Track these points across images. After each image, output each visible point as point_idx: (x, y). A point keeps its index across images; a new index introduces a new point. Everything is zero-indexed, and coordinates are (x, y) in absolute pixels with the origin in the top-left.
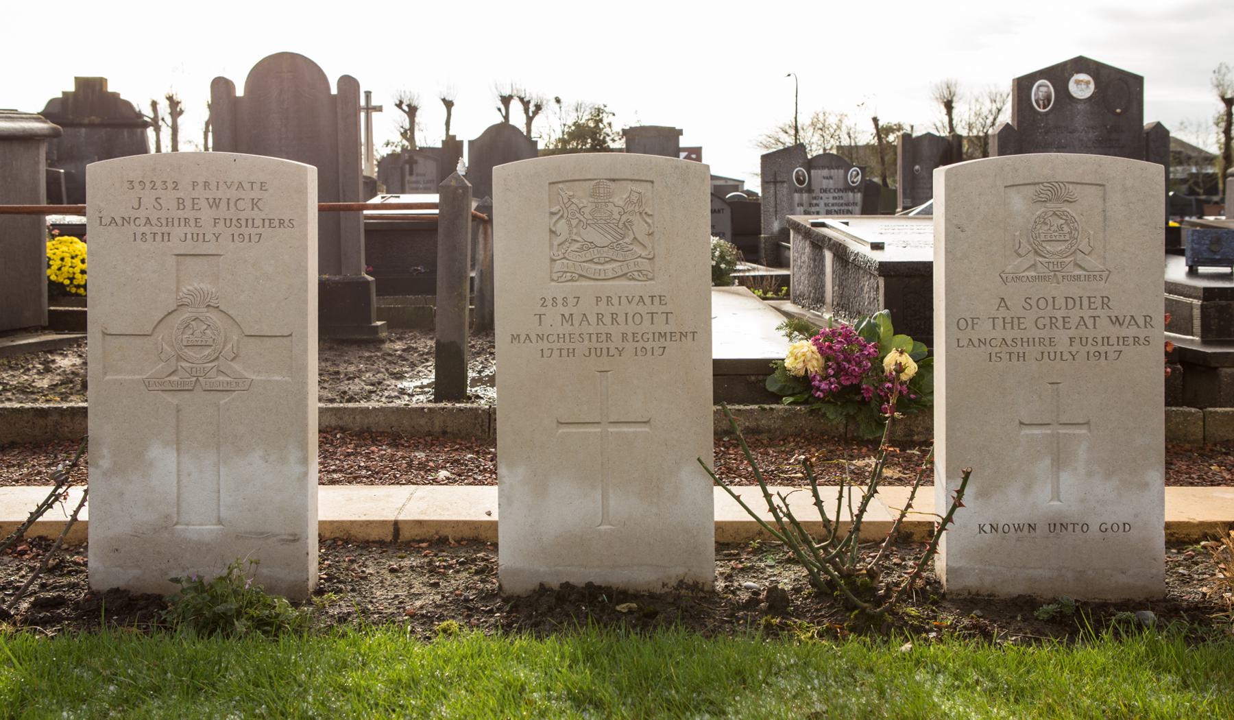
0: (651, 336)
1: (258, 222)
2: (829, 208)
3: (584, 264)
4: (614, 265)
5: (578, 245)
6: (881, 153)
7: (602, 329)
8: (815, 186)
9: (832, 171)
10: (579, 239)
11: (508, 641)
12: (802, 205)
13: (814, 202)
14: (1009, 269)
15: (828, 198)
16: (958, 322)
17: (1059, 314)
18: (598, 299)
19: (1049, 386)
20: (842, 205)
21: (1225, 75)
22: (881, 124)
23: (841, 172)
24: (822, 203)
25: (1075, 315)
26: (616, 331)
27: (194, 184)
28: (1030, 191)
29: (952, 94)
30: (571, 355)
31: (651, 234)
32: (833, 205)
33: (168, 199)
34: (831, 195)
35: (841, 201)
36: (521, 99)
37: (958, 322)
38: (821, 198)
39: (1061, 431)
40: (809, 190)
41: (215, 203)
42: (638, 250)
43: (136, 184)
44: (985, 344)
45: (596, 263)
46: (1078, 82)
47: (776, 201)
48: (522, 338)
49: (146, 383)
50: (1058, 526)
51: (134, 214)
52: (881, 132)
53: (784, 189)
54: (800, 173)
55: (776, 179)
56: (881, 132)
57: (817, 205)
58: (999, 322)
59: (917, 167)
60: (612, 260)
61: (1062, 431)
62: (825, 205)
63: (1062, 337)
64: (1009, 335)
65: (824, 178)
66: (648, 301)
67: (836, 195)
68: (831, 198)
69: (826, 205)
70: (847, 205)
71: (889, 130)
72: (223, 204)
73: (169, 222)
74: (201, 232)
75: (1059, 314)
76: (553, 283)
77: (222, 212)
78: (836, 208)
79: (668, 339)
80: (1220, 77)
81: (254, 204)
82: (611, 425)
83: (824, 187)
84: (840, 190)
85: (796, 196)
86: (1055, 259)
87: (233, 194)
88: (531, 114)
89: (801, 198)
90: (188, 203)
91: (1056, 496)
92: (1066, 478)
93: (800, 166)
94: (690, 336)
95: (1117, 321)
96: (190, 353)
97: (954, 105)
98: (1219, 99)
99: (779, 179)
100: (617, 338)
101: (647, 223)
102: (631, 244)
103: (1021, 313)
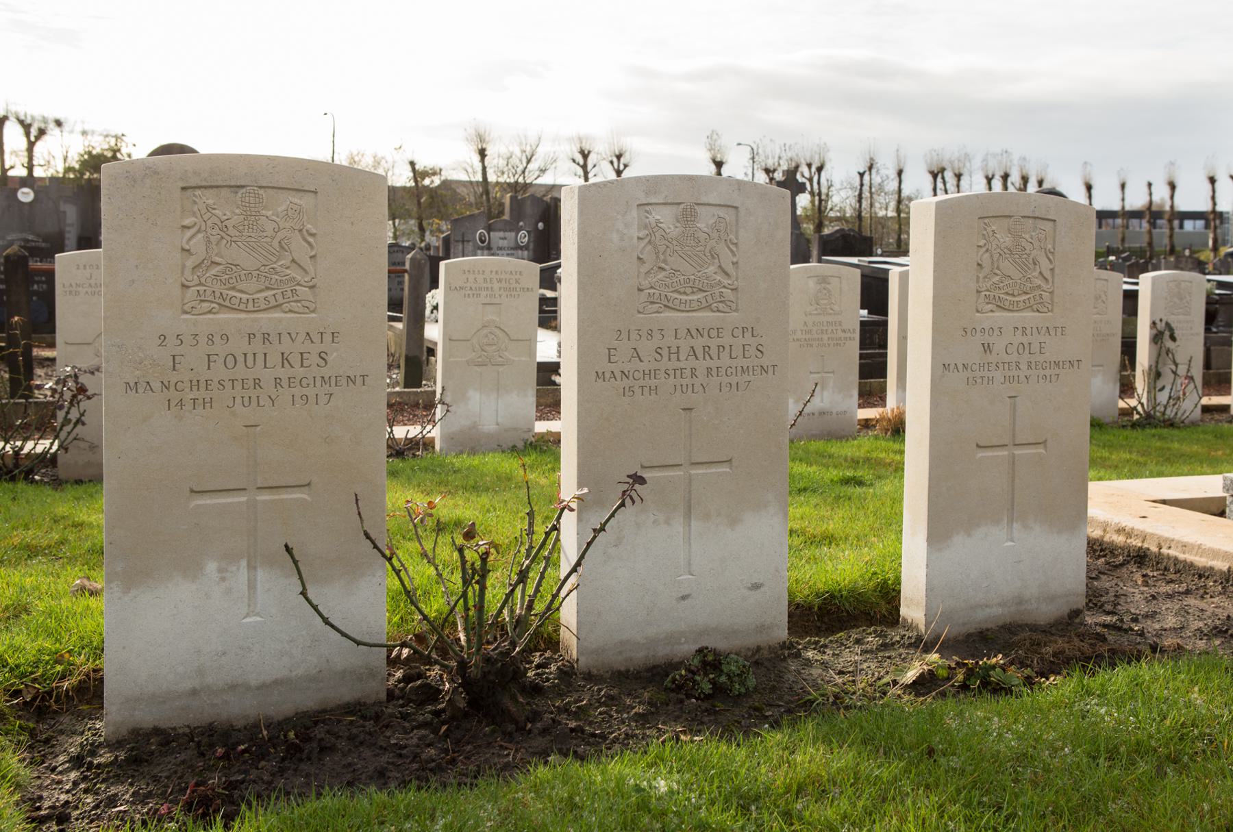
0: (1048, 365)
1: (518, 289)
3: (227, 292)
4: (700, 295)
6: (417, 196)
8: (494, 245)
9: (506, 233)
14: (808, 310)
16: (235, 363)
17: (824, 328)
18: (251, 336)
19: (244, 428)
21: (716, 140)
22: (417, 167)
23: (513, 234)
25: (830, 328)
26: (267, 376)
27: (491, 272)
28: (815, 279)
29: (481, 138)
30: (991, 382)
31: (1052, 270)
33: (480, 278)
36: (21, 122)
37: (235, 363)
39: (693, 472)
41: (500, 281)
44: (966, 369)
48: (952, 367)
49: (468, 362)
50: (822, 413)
51: (465, 285)
52: (418, 175)
55: (463, 238)
56: (418, 175)
58: (804, 332)
60: (700, 290)
61: (825, 375)
63: (825, 337)
64: (807, 337)
66: (317, 338)
67: (509, 252)
71: (425, 174)
72: (504, 282)
73: (480, 289)
75: (824, 328)
76: (978, 314)
77: (503, 285)
79: (751, 373)
80: (712, 143)
81: (517, 282)
83: (500, 246)
84: (512, 249)
87: (508, 276)
88: (33, 139)
90: (489, 280)
91: (822, 401)
92: (825, 393)
95: (844, 331)
96: (487, 348)
97: (486, 153)
98: (711, 161)
99: (466, 239)
100: (702, 373)
101: (309, 243)
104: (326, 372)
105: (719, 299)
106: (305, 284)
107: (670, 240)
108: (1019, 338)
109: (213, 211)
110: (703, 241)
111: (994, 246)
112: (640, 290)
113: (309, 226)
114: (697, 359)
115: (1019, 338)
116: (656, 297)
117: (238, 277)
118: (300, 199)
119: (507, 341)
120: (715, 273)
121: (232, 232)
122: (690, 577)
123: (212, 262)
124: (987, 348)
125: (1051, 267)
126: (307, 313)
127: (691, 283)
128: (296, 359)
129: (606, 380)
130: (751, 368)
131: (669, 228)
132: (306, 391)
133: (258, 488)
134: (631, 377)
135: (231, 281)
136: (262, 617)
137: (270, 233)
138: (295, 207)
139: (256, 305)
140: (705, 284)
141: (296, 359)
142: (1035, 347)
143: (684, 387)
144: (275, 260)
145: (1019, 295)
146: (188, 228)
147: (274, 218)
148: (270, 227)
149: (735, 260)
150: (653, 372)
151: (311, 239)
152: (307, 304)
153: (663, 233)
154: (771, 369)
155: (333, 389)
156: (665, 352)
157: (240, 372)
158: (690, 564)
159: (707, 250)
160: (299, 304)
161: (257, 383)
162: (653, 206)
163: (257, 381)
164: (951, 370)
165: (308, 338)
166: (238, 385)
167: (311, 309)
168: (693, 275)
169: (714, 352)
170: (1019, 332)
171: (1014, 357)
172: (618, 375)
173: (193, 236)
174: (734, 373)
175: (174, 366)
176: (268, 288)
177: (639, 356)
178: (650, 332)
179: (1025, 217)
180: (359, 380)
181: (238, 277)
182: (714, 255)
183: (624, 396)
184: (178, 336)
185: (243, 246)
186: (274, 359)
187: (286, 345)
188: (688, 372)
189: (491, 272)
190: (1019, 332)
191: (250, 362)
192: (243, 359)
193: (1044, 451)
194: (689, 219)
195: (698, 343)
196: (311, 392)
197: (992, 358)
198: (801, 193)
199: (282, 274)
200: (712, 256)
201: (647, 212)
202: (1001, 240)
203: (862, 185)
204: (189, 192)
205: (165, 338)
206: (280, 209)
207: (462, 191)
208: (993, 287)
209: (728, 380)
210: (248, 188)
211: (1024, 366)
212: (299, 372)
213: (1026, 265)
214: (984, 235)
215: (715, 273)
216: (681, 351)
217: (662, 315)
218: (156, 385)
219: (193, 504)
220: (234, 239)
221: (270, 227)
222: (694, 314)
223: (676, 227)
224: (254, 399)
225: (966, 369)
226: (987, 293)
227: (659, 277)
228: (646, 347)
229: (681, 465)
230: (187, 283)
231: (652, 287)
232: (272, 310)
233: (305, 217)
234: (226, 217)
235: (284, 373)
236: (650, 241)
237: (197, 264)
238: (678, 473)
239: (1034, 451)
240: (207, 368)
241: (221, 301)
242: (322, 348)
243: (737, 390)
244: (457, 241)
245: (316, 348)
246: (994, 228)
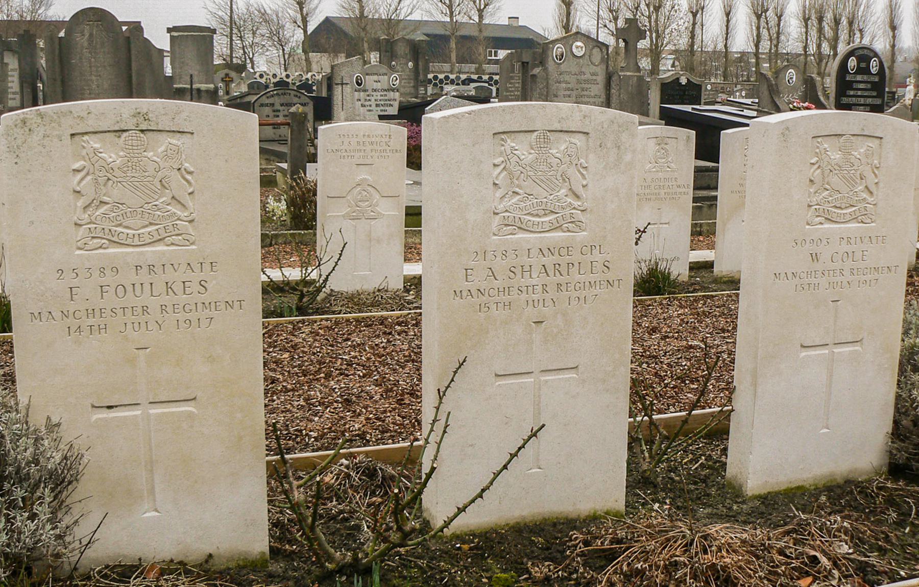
2: (378, 103)
3: (525, 217)
4: (552, 217)
12: (360, 100)
20: (386, 100)
24: (373, 99)
25: (667, 184)
26: (154, 303)
27: (364, 135)
32: (380, 100)
34: (379, 94)
35: (386, 98)
39: (152, 411)
41: (372, 143)
43: (341, 136)
46: (577, 47)
60: (851, 205)
62: (376, 100)
63: (662, 192)
64: (647, 191)
66: (197, 267)
67: (382, 93)
68: (379, 96)
69: (376, 100)
70: (389, 100)
74: (366, 154)
75: (662, 184)
76: (807, 227)
78: (382, 103)
79: (506, 294)
84: (385, 90)
86: (661, 164)
95: (679, 186)
101: (187, 181)
103: (650, 184)
104: (206, 298)
106: (185, 219)
107: (524, 166)
108: (845, 247)
109: (100, 155)
110: (554, 165)
111: (826, 163)
112: (496, 214)
113: (187, 165)
114: (548, 275)
115: (845, 247)
117: (124, 215)
118: (179, 140)
119: (378, 197)
120: (566, 196)
121: (117, 173)
122: (539, 470)
123: (101, 202)
124: (815, 257)
125: (876, 181)
126: (187, 246)
127: (544, 205)
128: (178, 287)
129: (464, 298)
130: (598, 283)
131: (524, 155)
133: (150, 403)
134: (487, 294)
135: (118, 218)
136: (159, 512)
137: (151, 171)
138: (174, 148)
139: (141, 239)
140: (557, 206)
141: (178, 287)
142: (858, 255)
143: (536, 301)
144: (157, 197)
146: (78, 171)
147: (155, 158)
148: (151, 168)
149: (584, 183)
150: (507, 289)
151: (189, 177)
152: (187, 237)
153: (518, 160)
154: (616, 283)
155: (214, 313)
156: (518, 271)
157: (130, 300)
158: (538, 460)
159: (559, 174)
160: (180, 238)
161: (145, 309)
162: (508, 135)
163: (145, 308)
164: (781, 278)
165: (189, 268)
166: (129, 312)
167: (191, 242)
168: (546, 198)
169: (564, 269)
170: (844, 242)
171: (838, 265)
172: (474, 292)
173: (82, 179)
174: (582, 288)
175: (72, 297)
176: (151, 224)
177: (494, 275)
178: (504, 252)
179: (854, 135)
181: (124, 215)
182: (565, 178)
183: (480, 312)
184: (74, 270)
185: (128, 186)
186: (160, 287)
187: (170, 275)
188: (539, 289)
189: (364, 135)
190: (844, 242)
191: (138, 292)
192: (132, 289)
193: (860, 349)
194: (542, 146)
195: (549, 260)
196: (193, 316)
197: (819, 266)
198: (641, 39)
199: (165, 210)
200: (564, 180)
201: (502, 140)
202: (832, 157)
203: (694, 24)
204: (77, 138)
205: (63, 272)
206: (160, 150)
207: (341, 24)
208: (822, 201)
209: (577, 294)
210: (130, 132)
211: (847, 273)
212: (183, 298)
213: (854, 180)
214: (816, 153)
215: (566, 196)
216: (532, 269)
217: (516, 236)
218: (57, 314)
219: (95, 417)
220: (119, 180)
221: (151, 168)
222: (547, 235)
223: (530, 153)
224: (143, 325)
226: (817, 207)
227: (513, 201)
228: (500, 265)
229: (532, 372)
230: (79, 222)
231: (507, 211)
232: (554, 231)
233: (184, 156)
234: (111, 160)
235: (167, 299)
236: (504, 168)
237: (87, 204)
238: (529, 380)
239: (851, 349)
240: (100, 298)
241: (110, 237)
242: (202, 276)
243: (585, 303)
244: (337, 84)
245: (196, 276)
246: (826, 146)
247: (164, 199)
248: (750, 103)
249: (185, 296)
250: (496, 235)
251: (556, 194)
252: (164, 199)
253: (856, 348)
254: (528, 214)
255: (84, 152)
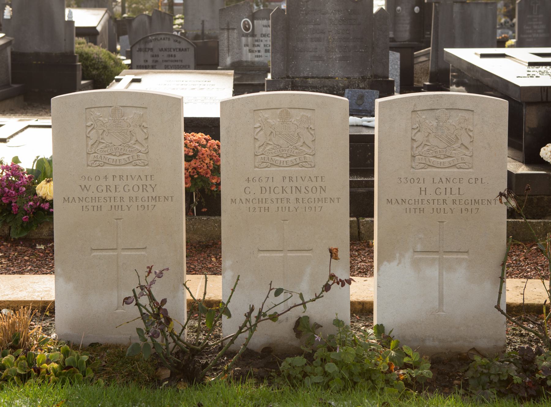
0: (470, 202)
3: (274, 158)
4: (125, 157)
5: (104, 145)
7: (285, 195)
10: (271, 143)
11: (271, 388)
13: (257, 43)
15: (266, 41)
16: (245, 188)
19: (438, 223)
38: (262, 41)
39: (289, 254)
40: (253, 35)
42: (304, 149)
44: (249, 202)
45: (114, 155)
47: (228, 42)
48: (394, 202)
53: (235, 34)
54: (246, 22)
57: (258, 46)
59: (399, 8)
65: (264, 26)
66: (314, 179)
69: (265, 46)
79: (324, 202)
82: (290, 252)
83: (264, 33)
85: (244, 39)
89: (247, 41)
93: (246, 18)
94: (336, 201)
101: (311, 134)
102: (302, 146)
105: (304, 161)
106: (143, 152)
116: (98, 158)
128: (113, 189)
129: (70, 202)
132: (467, 207)
139: (121, 162)
141: (113, 189)
144: (128, 141)
145: (120, 155)
161: (288, 200)
165: (139, 178)
173: (416, 133)
180: (336, 201)
187: (110, 181)
196: (469, 207)
199: (299, 149)
217: (103, 168)
225: (249, 202)
230: (89, 153)
232: (295, 166)
247: (458, 145)
248: (545, 93)
249: (451, 195)
250: (413, 168)
251: (295, 145)
252: (458, 145)
253: (143, 253)
254: (110, 154)
255: (260, 119)
